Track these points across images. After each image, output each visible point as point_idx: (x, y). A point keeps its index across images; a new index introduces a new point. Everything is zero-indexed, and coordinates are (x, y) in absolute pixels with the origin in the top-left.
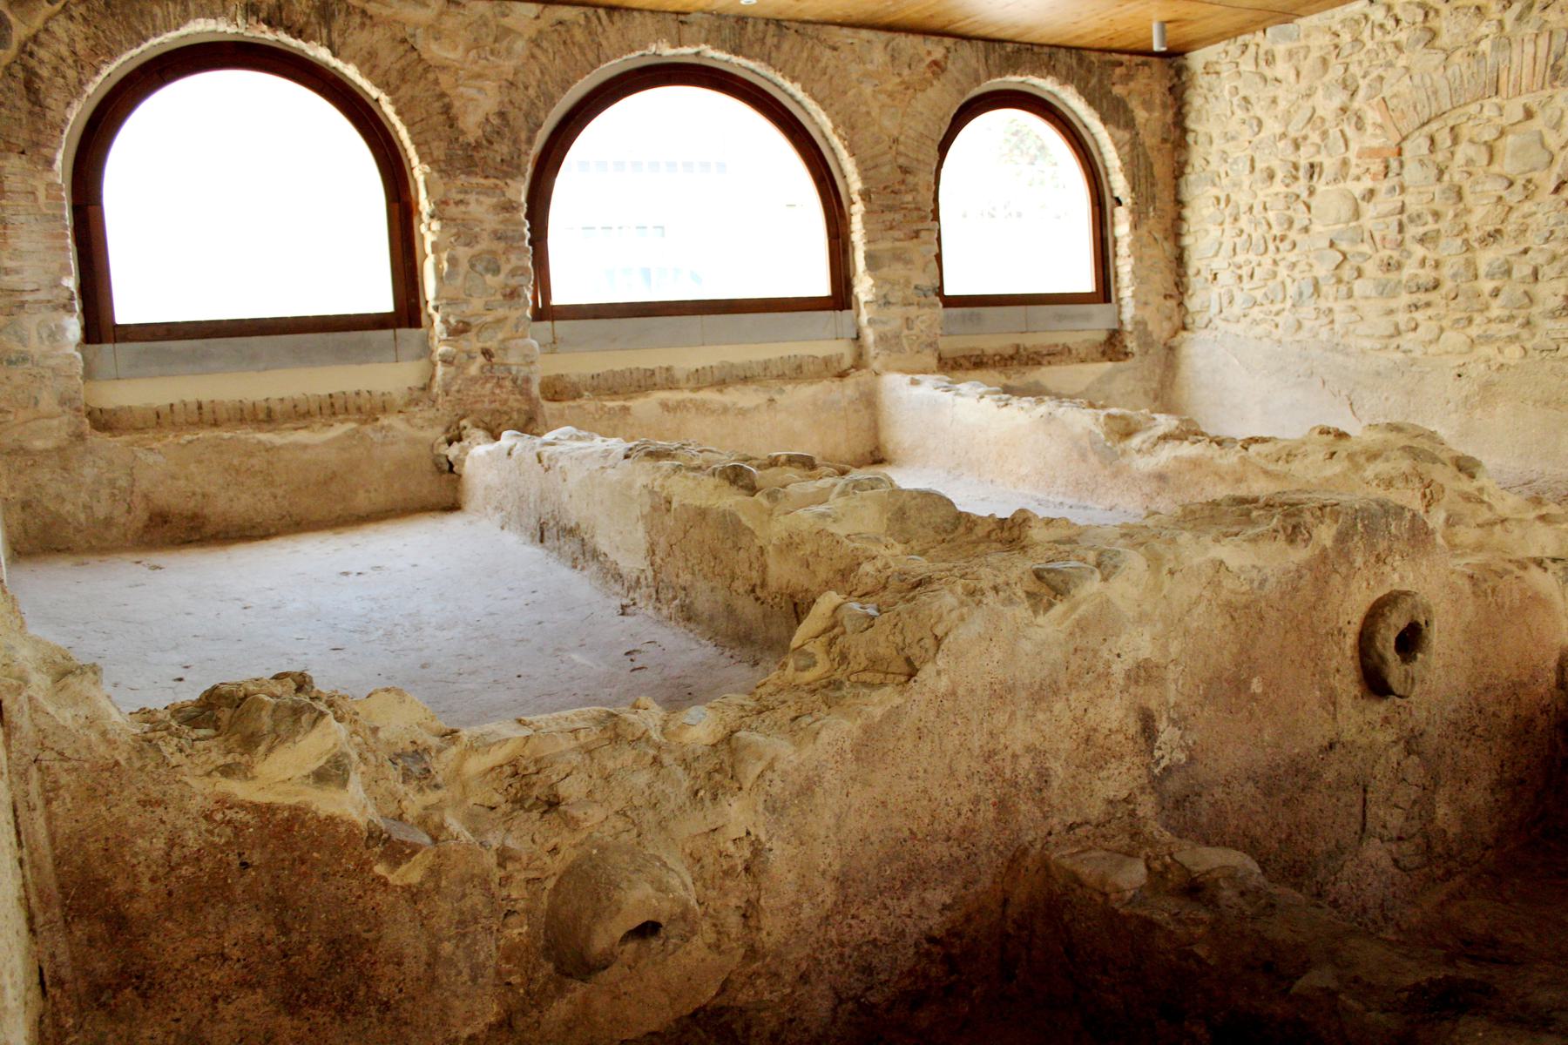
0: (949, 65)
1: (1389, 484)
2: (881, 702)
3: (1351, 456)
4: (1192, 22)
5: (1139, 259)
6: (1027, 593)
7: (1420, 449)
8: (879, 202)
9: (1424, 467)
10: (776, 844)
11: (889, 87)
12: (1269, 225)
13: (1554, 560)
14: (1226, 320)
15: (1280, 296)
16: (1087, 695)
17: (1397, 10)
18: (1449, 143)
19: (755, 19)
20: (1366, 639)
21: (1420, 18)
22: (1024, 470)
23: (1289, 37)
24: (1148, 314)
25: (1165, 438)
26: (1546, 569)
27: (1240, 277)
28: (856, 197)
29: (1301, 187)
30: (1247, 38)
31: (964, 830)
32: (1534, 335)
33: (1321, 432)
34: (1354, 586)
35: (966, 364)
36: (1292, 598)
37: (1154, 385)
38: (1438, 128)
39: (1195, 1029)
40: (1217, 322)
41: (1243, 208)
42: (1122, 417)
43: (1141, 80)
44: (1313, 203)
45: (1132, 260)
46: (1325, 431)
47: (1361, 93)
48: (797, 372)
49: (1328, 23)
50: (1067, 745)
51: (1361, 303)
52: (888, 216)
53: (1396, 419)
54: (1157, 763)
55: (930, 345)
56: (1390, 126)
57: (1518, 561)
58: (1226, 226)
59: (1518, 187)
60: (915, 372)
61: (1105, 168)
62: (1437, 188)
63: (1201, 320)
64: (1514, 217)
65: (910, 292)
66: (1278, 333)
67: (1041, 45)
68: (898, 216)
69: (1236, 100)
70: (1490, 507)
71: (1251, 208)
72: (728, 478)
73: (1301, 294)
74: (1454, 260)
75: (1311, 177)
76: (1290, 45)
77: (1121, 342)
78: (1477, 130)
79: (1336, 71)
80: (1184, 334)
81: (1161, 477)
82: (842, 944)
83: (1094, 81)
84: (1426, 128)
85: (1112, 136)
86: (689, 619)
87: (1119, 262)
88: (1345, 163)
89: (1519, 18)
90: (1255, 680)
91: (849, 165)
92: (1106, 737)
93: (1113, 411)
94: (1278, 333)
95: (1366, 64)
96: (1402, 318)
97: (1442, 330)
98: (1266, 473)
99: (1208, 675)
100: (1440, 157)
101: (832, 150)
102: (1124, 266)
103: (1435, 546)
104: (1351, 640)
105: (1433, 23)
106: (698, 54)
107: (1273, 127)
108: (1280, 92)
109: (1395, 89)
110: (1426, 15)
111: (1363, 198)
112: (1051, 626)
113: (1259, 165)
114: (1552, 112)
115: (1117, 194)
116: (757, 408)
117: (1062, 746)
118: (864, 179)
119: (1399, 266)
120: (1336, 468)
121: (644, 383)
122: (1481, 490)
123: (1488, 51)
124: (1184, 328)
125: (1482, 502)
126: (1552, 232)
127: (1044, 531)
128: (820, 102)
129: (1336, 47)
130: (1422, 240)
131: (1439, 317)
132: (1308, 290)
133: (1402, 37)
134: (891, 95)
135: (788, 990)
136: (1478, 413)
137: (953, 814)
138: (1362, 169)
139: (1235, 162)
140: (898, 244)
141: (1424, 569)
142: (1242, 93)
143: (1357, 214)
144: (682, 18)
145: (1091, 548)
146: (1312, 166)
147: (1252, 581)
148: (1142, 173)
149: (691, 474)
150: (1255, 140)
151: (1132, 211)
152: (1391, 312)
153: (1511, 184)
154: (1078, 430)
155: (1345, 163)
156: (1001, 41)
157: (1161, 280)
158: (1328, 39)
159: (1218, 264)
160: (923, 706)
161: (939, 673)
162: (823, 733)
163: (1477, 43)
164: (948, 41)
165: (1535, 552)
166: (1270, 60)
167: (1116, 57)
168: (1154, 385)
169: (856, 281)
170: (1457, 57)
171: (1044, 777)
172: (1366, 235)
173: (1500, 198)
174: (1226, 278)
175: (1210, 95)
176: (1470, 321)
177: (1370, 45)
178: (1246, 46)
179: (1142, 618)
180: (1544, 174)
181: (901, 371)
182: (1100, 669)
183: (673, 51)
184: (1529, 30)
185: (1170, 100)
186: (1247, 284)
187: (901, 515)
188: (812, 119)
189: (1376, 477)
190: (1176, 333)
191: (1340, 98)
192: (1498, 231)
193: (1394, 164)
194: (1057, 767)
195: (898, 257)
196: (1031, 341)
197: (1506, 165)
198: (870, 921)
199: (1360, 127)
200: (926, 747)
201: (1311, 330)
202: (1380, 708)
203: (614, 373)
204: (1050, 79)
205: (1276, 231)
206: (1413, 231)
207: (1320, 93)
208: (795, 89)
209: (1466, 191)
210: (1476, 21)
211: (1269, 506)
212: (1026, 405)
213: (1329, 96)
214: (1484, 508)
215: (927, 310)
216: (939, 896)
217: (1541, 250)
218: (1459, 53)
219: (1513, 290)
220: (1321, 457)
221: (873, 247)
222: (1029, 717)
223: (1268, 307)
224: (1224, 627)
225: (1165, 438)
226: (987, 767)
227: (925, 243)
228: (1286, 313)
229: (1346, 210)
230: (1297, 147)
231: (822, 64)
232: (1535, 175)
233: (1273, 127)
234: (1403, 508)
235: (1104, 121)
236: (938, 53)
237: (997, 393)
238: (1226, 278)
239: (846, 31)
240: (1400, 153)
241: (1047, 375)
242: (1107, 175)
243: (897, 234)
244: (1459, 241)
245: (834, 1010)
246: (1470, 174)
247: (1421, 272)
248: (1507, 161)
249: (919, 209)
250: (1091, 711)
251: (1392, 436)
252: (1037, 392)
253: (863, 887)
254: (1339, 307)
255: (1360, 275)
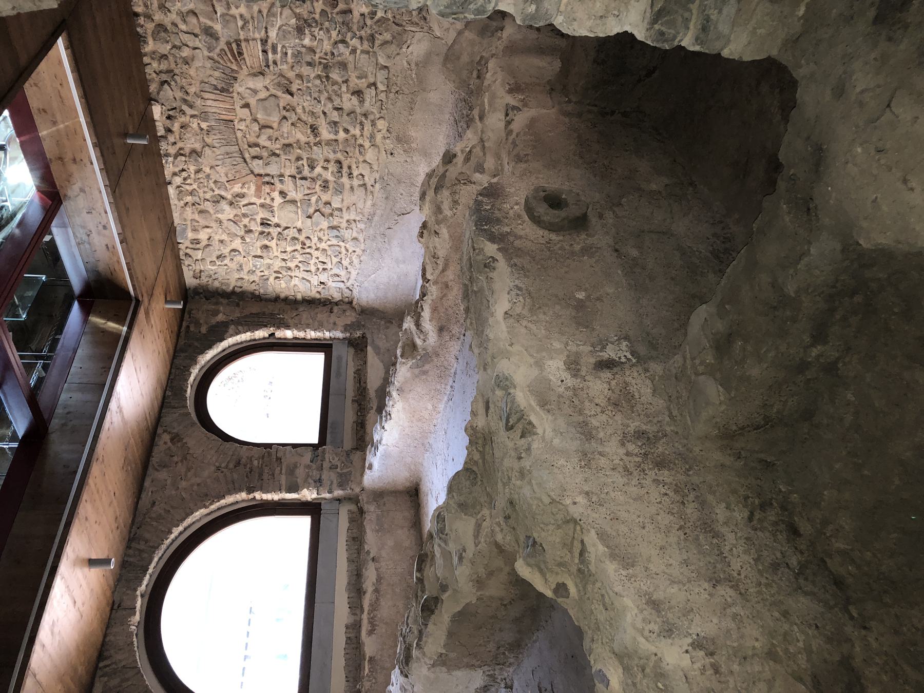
0: (175, 431)
1: (456, 202)
2: (594, 545)
3: (438, 222)
4: (168, 283)
5: (308, 326)
6: (521, 437)
7: (437, 183)
8: (254, 478)
9: (447, 182)
10: (694, 630)
11: (183, 470)
12: (294, 251)
13: (507, 115)
14: (348, 279)
15: (337, 248)
16: (587, 403)
17: (177, 170)
18: (257, 149)
19: (125, 555)
20: (551, 227)
21: (183, 158)
22: (430, 407)
23: (185, 230)
24: (341, 322)
25: (418, 325)
26: (513, 120)
27: (324, 269)
28: (251, 496)
29: (274, 231)
30: (181, 253)
31: (676, 492)
32: (372, 113)
33: (422, 237)
34: (522, 233)
35: (361, 432)
36: (528, 271)
37: (383, 322)
38: (245, 155)
39: (813, 354)
40: (348, 284)
41: (283, 264)
42: (403, 348)
43: (201, 317)
44: (284, 225)
45: (308, 330)
46: (421, 235)
47: (223, 193)
48: (357, 540)
49: (178, 208)
50: (619, 417)
51: (345, 204)
52: (265, 476)
53: (417, 196)
54: (629, 360)
55: (348, 455)
56: (244, 180)
57: (507, 135)
58: (293, 274)
59: (287, 114)
60: (363, 466)
61: (250, 341)
62: (283, 157)
63: (347, 293)
64: (304, 118)
65: (314, 466)
66: (359, 251)
67: (170, 373)
68: (266, 470)
69: (218, 263)
70: (473, 147)
71: (284, 260)
72: (429, 616)
73: (337, 236)
74: (325, 152)
75: (269, 225)
76: (189, 230)
77: (355, 339)
78: (252, 133)
79: (208, 206)
80: (354, 303)
81: (441, 330)
82: (760, 584)
83: (196, 344)
84: (248, 160)
85: (231, 336)
86: (519, 646)
87: (309, 337)
88: (262, 206)
89: (191, 107)
90: (577, 296)
91: (230, 499)
92: (613, 392)
93: (399, 352)
94: (359, 251)
95: (206, 189)
96: (356, 182)
97: (365, 161)
98: (443, 271)
99: (574, 325)
100: (265, 154)
101: (219, 509)
102: (312, 334)
103: (497, 183)
104: (553, 236)
105: (187, 151)
106: (142, 596)
107: (237, 244)
108: (217, 237)
109: (222, 175)
110: (182, 155)
111: (285, 198)
112: (543, 423)
113: (259, 253)
114: (247, 93)
115: (267, 335)
116: (377, 569)
117: (620, 422)
118: (241, 490)
119: (326, 181)
120: (444, 232)
121: (354, 644)
122: (462, 151)
123: (208, 124)
124: (351, 303)
125: (470, 151)
126: (315, 99)
127: (479, 417)
128: (187, 515)
129: (193, 204)
130: (312, 168)
131: (357, 163)
132: (335, 232)
133: (192, 168)
134: (189, 470)
135: (795, 627)
136: (414, 145)
137: (665, 498)
138: (268, 197)
139: (255, 266)
140: (283, 471)
141: (513, 190)
142: (215, 259)
143: (294, 202)
144: (116, 607)
145: (493, 391)
146: (262, 224)
147: (518, 295)
148: (256, 319)
149: (424, 639)
150: (243, 254)
151: (279, 328)
152: (352, 188)
153: (285, 118)
154: (409, 375)
155: (262, 206)
156: (164, 397)
157: (322, 315)
158: (189, 210)
159: (315, 281)
160: (597, 516)
161: (575, 503)
162: (616, 590)
163: (202, 129)
164: (160, 431)
165: (502, 125)
166: (197, 241)
167: (183, 329)
168: (383, 322)
169: (304, 499)
170: (208, 140)
171: (640, 435)
172: (306, 197)
173: (292, 124)
174: (323, 277)
175: (214, 277)
176: (361, 146)
177: (195, 186)
178: (186, 254)
179: (539, 364)
180: (282, 100)
181: (362, 475)
182: (570, 393)
183: (138, 613)
184: (199, 102)
185: (213, 300)
186: (329, 266)
187: (463, 507)
188: (198, 521)
189: (451, 210)
190: (353, 308)
191: (224, 205)
192: (311, 127)
193: (267, 179)
194: (633, 425)
195: (291, 471)
196: (350, 393)
197: (274, 119)
198: (740, 561)
199: (243, 196)
200: (623, 515)
201: (358, 232)
202: (593, 220)
203: (347, 665)
204: (192, 370)
205: (298, 247)
206: (306, 172)
207: (220, 216)
208: (176, 531)
209: (286, 142)
210: (189, 129)
211: (471, 279)
212: (391, 403)
213: (222, 211)
214: (474, 150)
215: (327, 456)
216: (721, 513)
217: (325, 105)
218: (206, 139)
219: (345, 122)
220: (437, 239)
221: (284, 487)
222: (602, 442)
223: (343, 256)
224: (545, 313)
225: (418, 325)
226: (635, 473)
227: (285, 454)
228: (347, 246)
229: (291, 208)
230: (250, 231)
231: (162, 512)
232: (282, 105)
233: (237, 244)
234: (476, 200)
235: (222, 339)
236: (166, 437)
237: (381, 418)
238: (323, 277)
239: (143, 496)
240: (261, 175)
241: (373, 381)
242: (255, 340)
243: (277, 470)
244: (315, 148)
245: (806, 594)
246: (277, 139)
247: (330, 170)
248: (272, 119)
249: (263, 457)
250: (597, 401)
251: (428, 198)
252: (383, 394)
253: (719, 566)
254: (346, 216)
255: (330, 204)
